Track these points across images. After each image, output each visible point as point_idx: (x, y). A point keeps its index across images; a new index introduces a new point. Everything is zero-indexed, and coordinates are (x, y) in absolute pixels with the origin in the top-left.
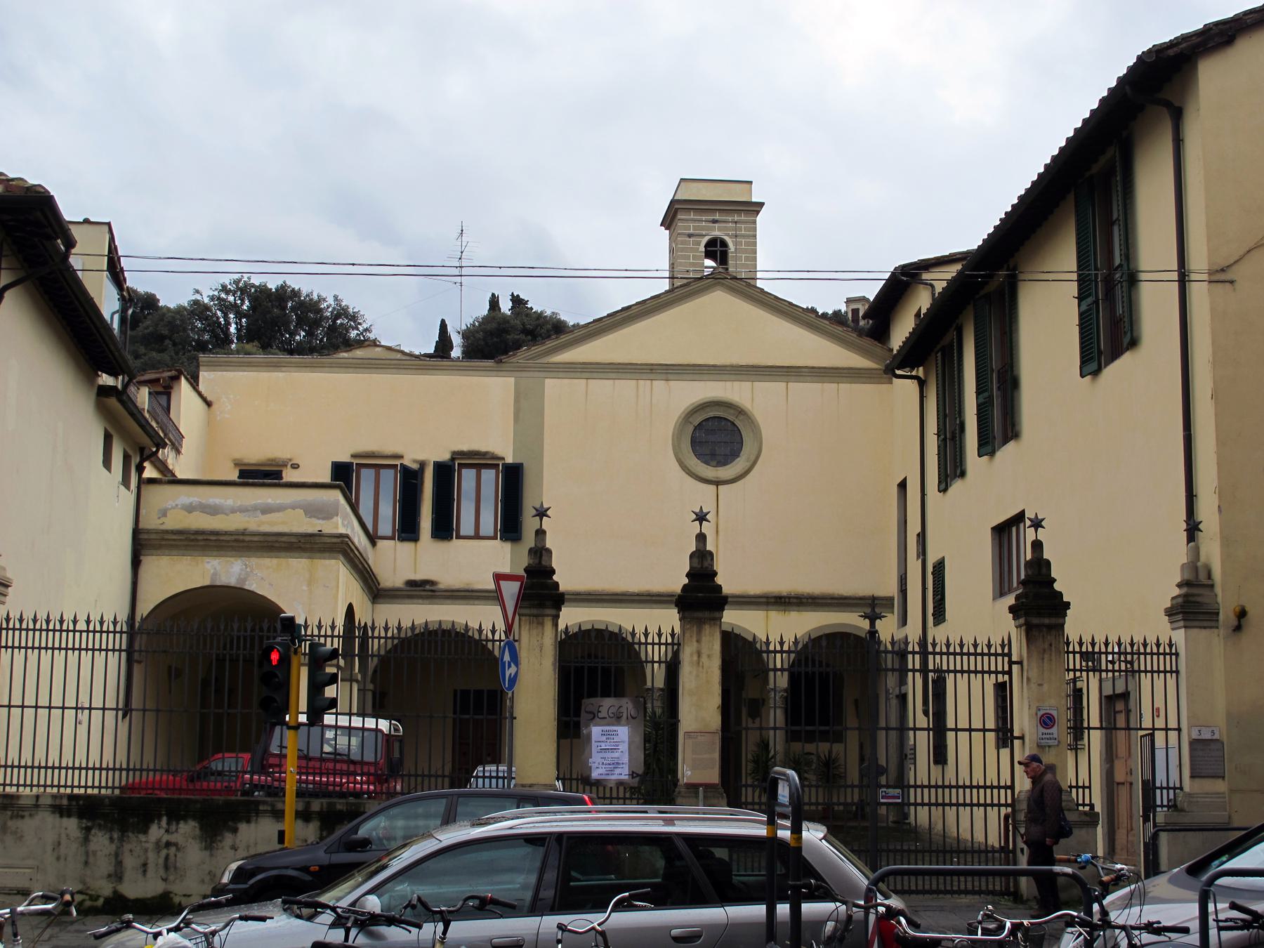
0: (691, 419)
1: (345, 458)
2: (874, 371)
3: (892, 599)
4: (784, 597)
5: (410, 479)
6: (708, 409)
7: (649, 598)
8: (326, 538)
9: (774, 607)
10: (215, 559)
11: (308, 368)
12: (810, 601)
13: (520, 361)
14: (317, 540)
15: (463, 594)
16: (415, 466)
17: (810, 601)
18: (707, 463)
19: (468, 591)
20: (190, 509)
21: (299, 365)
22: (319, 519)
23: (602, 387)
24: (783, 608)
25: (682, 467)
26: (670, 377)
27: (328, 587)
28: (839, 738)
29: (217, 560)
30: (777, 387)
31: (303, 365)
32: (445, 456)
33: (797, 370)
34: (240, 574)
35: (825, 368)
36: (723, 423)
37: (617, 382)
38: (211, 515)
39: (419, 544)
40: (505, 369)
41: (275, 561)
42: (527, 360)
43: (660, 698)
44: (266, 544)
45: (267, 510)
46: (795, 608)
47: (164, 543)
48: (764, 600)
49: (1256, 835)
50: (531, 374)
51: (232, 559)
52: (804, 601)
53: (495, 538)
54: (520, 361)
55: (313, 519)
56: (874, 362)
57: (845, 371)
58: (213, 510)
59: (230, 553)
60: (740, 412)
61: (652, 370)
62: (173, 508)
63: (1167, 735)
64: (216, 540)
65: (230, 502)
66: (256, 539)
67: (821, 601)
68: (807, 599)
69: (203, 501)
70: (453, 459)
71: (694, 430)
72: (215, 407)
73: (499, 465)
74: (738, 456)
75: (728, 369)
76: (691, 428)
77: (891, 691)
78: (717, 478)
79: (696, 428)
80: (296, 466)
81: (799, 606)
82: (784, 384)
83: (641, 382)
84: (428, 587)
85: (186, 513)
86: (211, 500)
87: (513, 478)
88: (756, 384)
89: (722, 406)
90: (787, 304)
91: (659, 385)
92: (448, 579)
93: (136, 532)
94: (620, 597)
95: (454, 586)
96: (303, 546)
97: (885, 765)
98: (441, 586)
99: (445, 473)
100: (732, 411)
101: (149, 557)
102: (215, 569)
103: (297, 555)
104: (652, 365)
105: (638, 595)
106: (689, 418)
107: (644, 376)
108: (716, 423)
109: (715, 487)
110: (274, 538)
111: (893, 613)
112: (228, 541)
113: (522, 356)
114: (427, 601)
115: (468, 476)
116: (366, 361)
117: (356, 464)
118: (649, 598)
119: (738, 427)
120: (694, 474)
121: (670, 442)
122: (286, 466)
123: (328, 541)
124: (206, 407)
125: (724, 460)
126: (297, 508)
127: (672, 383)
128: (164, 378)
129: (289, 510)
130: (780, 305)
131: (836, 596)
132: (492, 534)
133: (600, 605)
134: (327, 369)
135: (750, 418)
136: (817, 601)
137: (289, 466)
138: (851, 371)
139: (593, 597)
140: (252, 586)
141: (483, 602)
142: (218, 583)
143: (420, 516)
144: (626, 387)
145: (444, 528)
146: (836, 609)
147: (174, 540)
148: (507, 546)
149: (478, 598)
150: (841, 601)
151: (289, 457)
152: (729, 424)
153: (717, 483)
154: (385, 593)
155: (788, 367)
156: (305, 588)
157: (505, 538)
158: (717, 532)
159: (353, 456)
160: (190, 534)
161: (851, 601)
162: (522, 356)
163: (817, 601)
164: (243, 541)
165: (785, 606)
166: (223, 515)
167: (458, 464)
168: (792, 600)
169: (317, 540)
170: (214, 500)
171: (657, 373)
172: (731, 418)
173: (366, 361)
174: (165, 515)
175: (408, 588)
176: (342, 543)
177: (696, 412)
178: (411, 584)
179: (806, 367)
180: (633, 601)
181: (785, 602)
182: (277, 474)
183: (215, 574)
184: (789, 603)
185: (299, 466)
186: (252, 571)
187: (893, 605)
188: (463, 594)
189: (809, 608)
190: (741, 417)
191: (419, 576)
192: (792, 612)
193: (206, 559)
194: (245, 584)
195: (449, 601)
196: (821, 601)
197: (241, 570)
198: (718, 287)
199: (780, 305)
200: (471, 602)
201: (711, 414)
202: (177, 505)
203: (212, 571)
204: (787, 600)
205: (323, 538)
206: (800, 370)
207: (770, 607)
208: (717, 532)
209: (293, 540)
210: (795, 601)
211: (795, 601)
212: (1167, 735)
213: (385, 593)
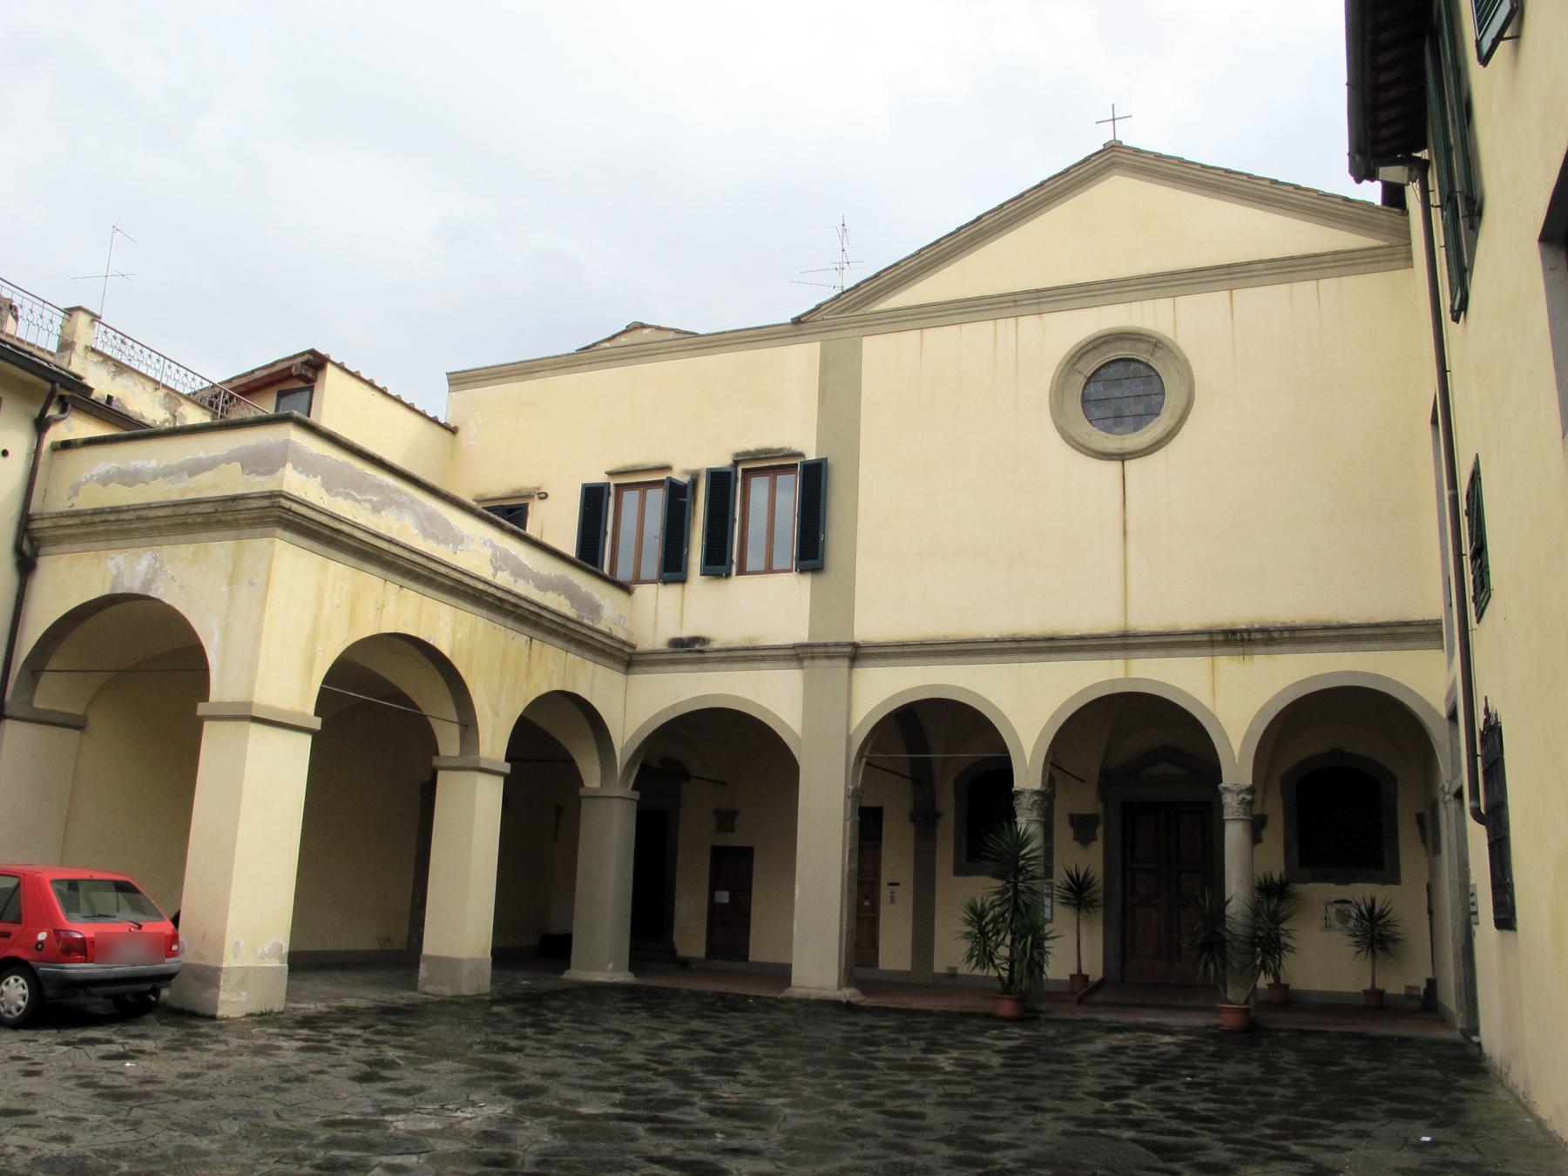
0: (1078, 367)
1: (599, 477)
2: (1379, 251)
3: (1438, 623)
4: (1241, 631)
5: (678, 497)
6: (1105, 348)
7: (1014, 645)
8: (253, 501)
9: (1226, 650)
10: (120, 554)
11: (565, 369)
12: (1286, 635)
13: (825, 317)
14: (242, 505)
15: (741, 653)
16: (685, 479)
17: (1286, 635)
18: (1108, 430)
19: (747, 649)
20: (105, 480)
21: (553, 367)
22: (259, 474)
23: (941, 338)
24: (1241, 650)
25: (1064, 439)
26: (1044, 307)
27: (254, 584)
28: (1393, 878)
29: (123, 554)
30: (1214, 301)
31: (557, 366)
32: (722, 461)
33: (1244, 268)
34: (146, 574)
35: (1292, 258)
36: (1132, 368)
37: (965, 326)
38: (129, 486)
39: (687, 586)
40: (805, 332)
41: (192, 548)
42: (835, 314)
43: (1035, 807)
44: (176, 520)
45: (196, 468)
46: (1262, 649)
47: (59, 532)
48: (1205, 638)
49: (360, 549)
50: (839, 334)
51: (139, 551)
52: (1276, 635)
53: (791, 571)
54: (825, 317)
55: (253, 476)
56: (1376, 239)
57: (1328, 258)
58: (131, 478)
59: (137, 542)
60: (1156, 343)
61: (1015, 301)
62: (87, 481)
63: (1118, 119)
64: (116, 521)
65: (153, 464)
66: (162, 513)
67: (1306, 634)
68: (1282, 631)
69: (122, 467)
70: (736, 463)
71: (1086, 384)
72: (461, 433)
73: (797, 464)
74: (1157, 415)
75: (1133, 282)
76: (1080, 381)
77: (1446, 788)
78: (1121, 449)
79: (1089, 380)
80: (543, 495)
81: (1267, 645)
82: (1225, 294)
83: (1001, 323)
84: (697, 647)
85: (100, 486)
86: (132, 464)
87: (814, 478)
88: (1180, 300)
89: (1126, 339)
90: (1222, 173)
91: (1029, 323)
92: (724, 630)
93: (25, 521)
94: (970, 647)
95: (732, 643)
96: (223, 518)
97: (47, 668)
98: (715, 645)
99: (720, 482)
100: (1143, 346)
101: (49, 558)
102: (119, 568)
103: (219, 534)
104: (1015, 294)
105: (996, 641)
106: (1075, 364)
107: (1006, 312)
108: (1121, 370)
109: (1120, 463)
110: (184, 510)
111: (1442, 648)
112: (130, 521)
113: (830, 309)
114: (696, 668)
115: (759, 487)
116: (631, 349)
117: (617, 486)
118: (1014, 645)
119: (1155, 371)
120: (1083, 446)
121: (1047, 403)
122: (533, 497)
123: (255, 506)
124: (447, 434)
125: (1140, 422)
126: (233, 461)
127: (1047, 317)
128: (296, 365)
129: (223, 464)
130: (1209, 175)
131: (1334, 624)
132: (789, 568)
133: (940, 660)
134: (585, 366)
135: (1171, 352)
136: (1298, 634)
137: (536, 497)
138: (1337, 257)
139: (929, 648)
140: (165, 592)
141: (770, 665)
142: (119, 591)
143: (688, 547)
144: (978, 332)
145: (718, 562)
146: (1336, 646)
147: (70, 526)
148: (806, 581)
149: (763, 659)
150: (1341, 633)
151: (537, 485)
152: (1142, 367)
153: (1122, 457)
154: (641, 658)
155: (1229, 266)
156: (224, 589)
157: (802, 570)
158: (1125, 533)
159: (611, 474)
160: (87, 514)
161: (1355, 632)
162: (830, 309)
163: (1298, 634)
164: (147, 519)
165: (1243, 646)
166: (143, 484)
167: (743, 469)
168: (1254, 636)
169: (242, 505)
170: (135, 462)
171: (1022, 305)
172: (1143, 357)
173: (631, 349)
174: (76, 494)
175: (672, 649)
176: (273, 507)
177: (1085, 354)
178: (677, 643)
179: (1260, 262)
180: (991, 652)
181: (1242, 640)
182: (519, 509)
183: (118, 576)
184: (1250, 640)
185: (547, 496)
186: (161, 568)
187: (1441, 633)
188: (741, 653)
189: (1285, 648)
190: (1159, 353)
191: (686, 633)
192: (1256, 657)
193: (111, 553)
194: (151, 589)
195: (724, 666)
196: (1306, 634)
197: (150, 566)
198: (1114, 170)
199: (1209, 175)
200: (755, 665)
201: (1112, 356)
202: (92, 476)
203: (114, 572)
204: (1245, 636)
205: (250, 501)
206: (1250, 267)
207: (1217, 650)
208: (1125, 533)
209: (209, 508)
210: (1259, 636)
211: (1259, 636)
212: (1118, 119)
213: (641, 658)
